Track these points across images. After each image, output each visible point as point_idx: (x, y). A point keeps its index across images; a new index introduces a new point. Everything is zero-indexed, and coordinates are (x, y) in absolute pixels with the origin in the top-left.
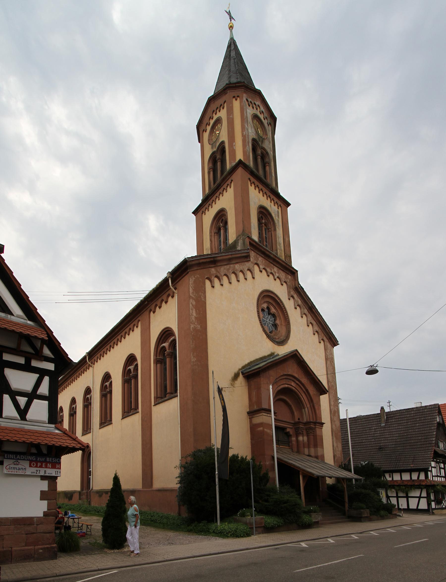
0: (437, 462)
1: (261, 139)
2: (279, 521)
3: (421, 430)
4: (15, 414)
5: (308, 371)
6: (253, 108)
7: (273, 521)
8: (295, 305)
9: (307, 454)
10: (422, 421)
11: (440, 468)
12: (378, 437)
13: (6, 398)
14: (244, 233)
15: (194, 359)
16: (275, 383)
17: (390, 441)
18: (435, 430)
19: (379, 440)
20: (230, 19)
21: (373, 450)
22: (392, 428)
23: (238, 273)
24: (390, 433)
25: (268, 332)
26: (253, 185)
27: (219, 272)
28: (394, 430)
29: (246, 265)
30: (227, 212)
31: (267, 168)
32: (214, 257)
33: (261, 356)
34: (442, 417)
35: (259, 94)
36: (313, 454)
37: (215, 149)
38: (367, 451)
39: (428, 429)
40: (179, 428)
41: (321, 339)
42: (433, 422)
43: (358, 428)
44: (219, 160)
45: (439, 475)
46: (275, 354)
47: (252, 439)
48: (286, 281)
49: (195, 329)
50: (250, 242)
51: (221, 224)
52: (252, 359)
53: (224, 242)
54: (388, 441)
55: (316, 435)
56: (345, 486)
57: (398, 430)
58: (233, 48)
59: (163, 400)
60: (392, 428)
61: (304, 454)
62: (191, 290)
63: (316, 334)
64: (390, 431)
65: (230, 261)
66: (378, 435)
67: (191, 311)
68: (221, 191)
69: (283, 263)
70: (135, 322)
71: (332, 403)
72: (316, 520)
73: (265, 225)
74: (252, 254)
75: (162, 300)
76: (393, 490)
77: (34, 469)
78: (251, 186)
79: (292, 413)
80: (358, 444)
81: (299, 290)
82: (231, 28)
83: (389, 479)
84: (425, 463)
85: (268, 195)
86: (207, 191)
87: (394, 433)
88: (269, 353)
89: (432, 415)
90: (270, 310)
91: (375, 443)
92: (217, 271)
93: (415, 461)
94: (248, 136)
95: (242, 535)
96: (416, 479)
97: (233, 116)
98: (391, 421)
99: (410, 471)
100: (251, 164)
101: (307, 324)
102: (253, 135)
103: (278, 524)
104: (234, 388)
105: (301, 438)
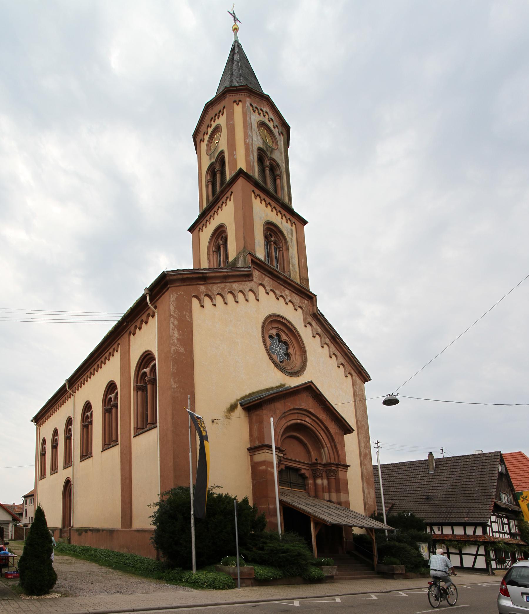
0: (498, 517)
1: (269, 149)
2: (276, 573)
3: (479, 479)
6: (259, 114)
7: (268, 573)
8: (313, 333)
9: (328, 499)
10: (480, 470)
11: (503, 524)
12: (425, 486)
14: (247, 250)
15: (174, 385)
16: (284, 417)
17: (440, 491)
18: (496, 481)
19: (426, 489)
20: (235, 20)
21: (419, 500)
22: (443, 477)
23: (236, 293)
24: (439, 482)
25: (278, 362)
26: (258, 198)
27: (210, 291)
28: (445, 479)
29: (247, 285)
31: (278, 181)
32: (202, 273)
33: (267, 387)
34: (505, 466)
35: (267, 99)
37: (213, 160)
38: (412, 500)
39: (487, 479)
40: (159, 462)
41: (347, 372)
42: (494, 472)
43: (401, 475)
44: (219, 172)
45: (501, 531)
47: (253, 479)
48: (301, 305)
49: (177, 352)
50: (252, 260)
53: (223, 261)
54: (438, 491)
55: (339, 479)
56: (374, 538)
57: (450, 479)
59: (143, 431)
60: (443, 477)
61: (323, 499)
62: (172, 308)
63: (341, 366)
64: (440, 480)
65: (225, 279)
66: (425, 483)
67: (171, 331)
68: (219, 204)
69: (297, 286)
70: (115, 346)
71: (362, 445)
72: (329, 575)
73: (275, 243)
74: (256, 274)
75: (142, 321)
76: (443, 545)
78: (256, 199)
79: (309, 452)
80: (401, 493)
81: (319, 317)
82: (235, 31)
83: (438, 532)
84: (482, 516)
85: (278, 211)
86: (205, 206)
87: (444, 482)
88: (278, 384)
89: (492, 463)
90: (279, 336)
91: (421, 492)
92: (207, 289)
93: (470, 514)
94: (252, 144)
95: (221, 587)
96: (472, 534)
97: (234, 122)
98: (442, 468)
99: (465, 525)
101: (330, 355)
102: (258, 144)
103: (275, 577)
104: (230, 421)
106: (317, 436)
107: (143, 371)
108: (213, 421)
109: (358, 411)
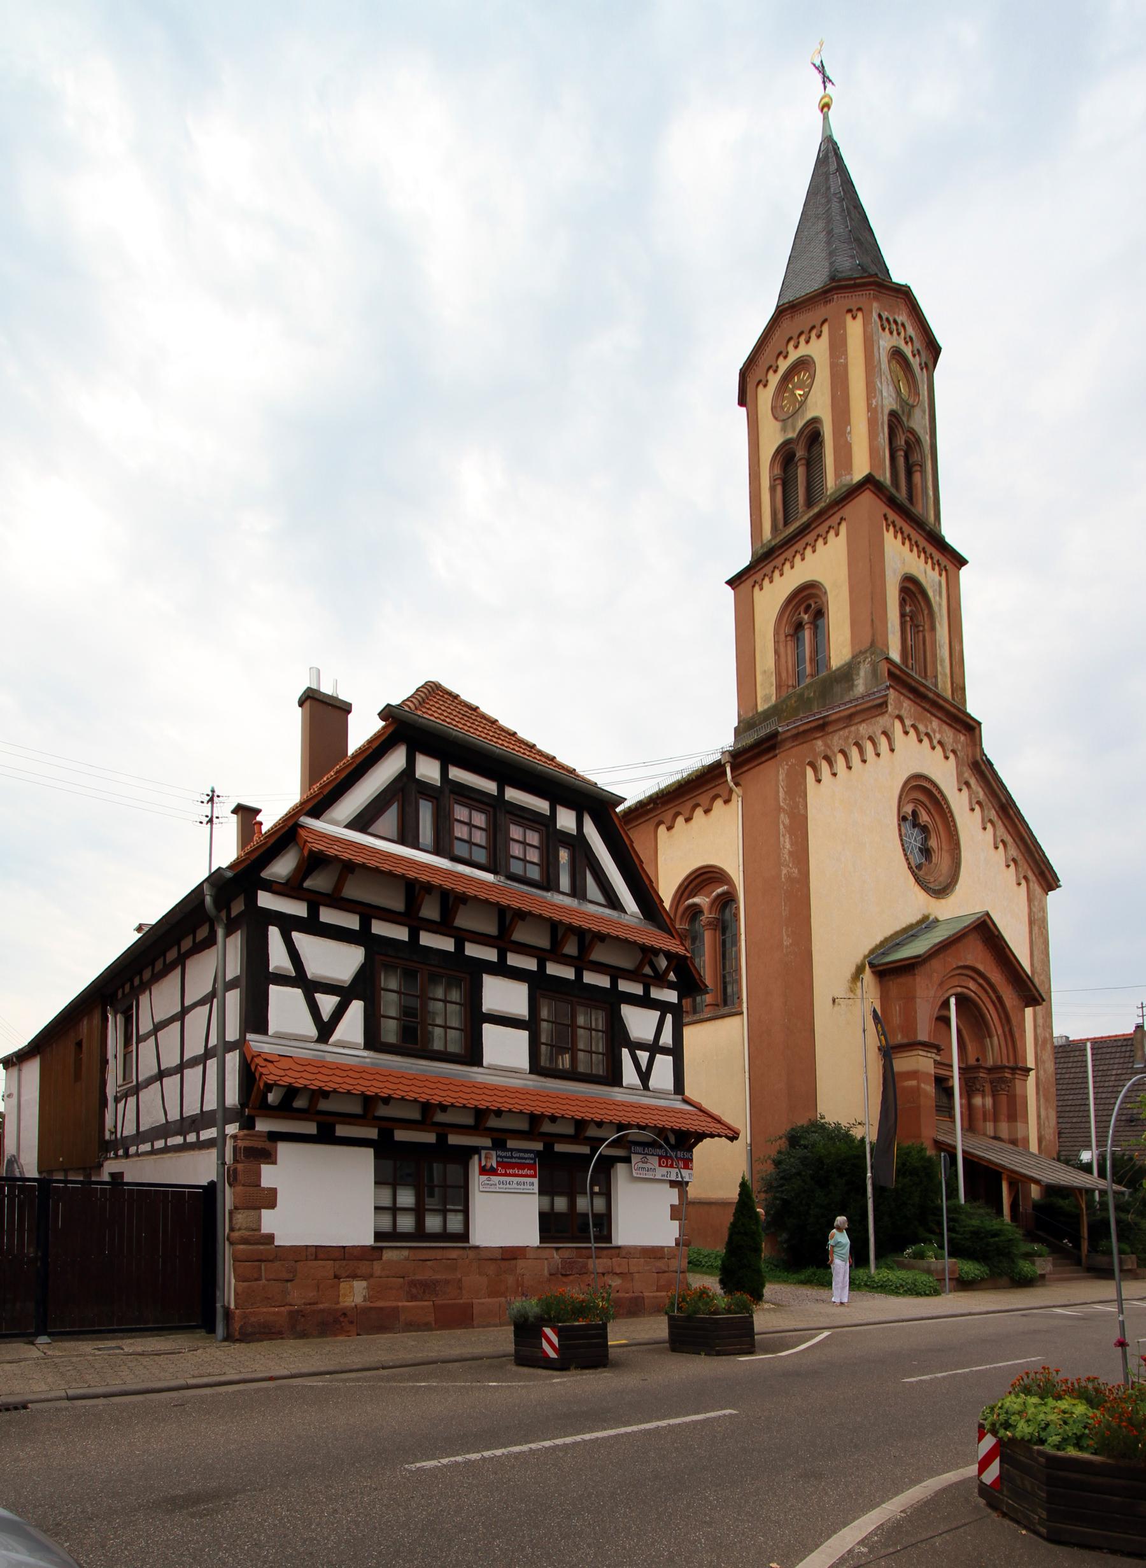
4: (636, 1081)
5: (1007, 958)
6: (891, 333)
9: (992, 1134)
13: (625, 1052)
14: (870, 646)
20: (824, 82)
26: (891, 529)
27: (829, 747)
30: (826, 593)
31: (917, 477)
35: (904, 294)
36: (1004, 1134)
46: (931, 918)
49: (789, 878)
51: (806, 617)
52: (889, 932)
55: (1015, 1096)
56: (1084, 1206)
58: (833, 167)
61: (985, 1134)
62: (782, 794)
68: (810, 538)
73: (911, 619)
77: (664, 1170)
81: (983, 767)
82: (825, 110)
88: (919, 917)
90: (923, 816)
97: (846, 358)
100: (886, 477)
101: (995, 843)
105: (978, 1101)
106: (982, 1016)
107: (690, 901)
108: (834, 1001)
109: (1035, 953)
